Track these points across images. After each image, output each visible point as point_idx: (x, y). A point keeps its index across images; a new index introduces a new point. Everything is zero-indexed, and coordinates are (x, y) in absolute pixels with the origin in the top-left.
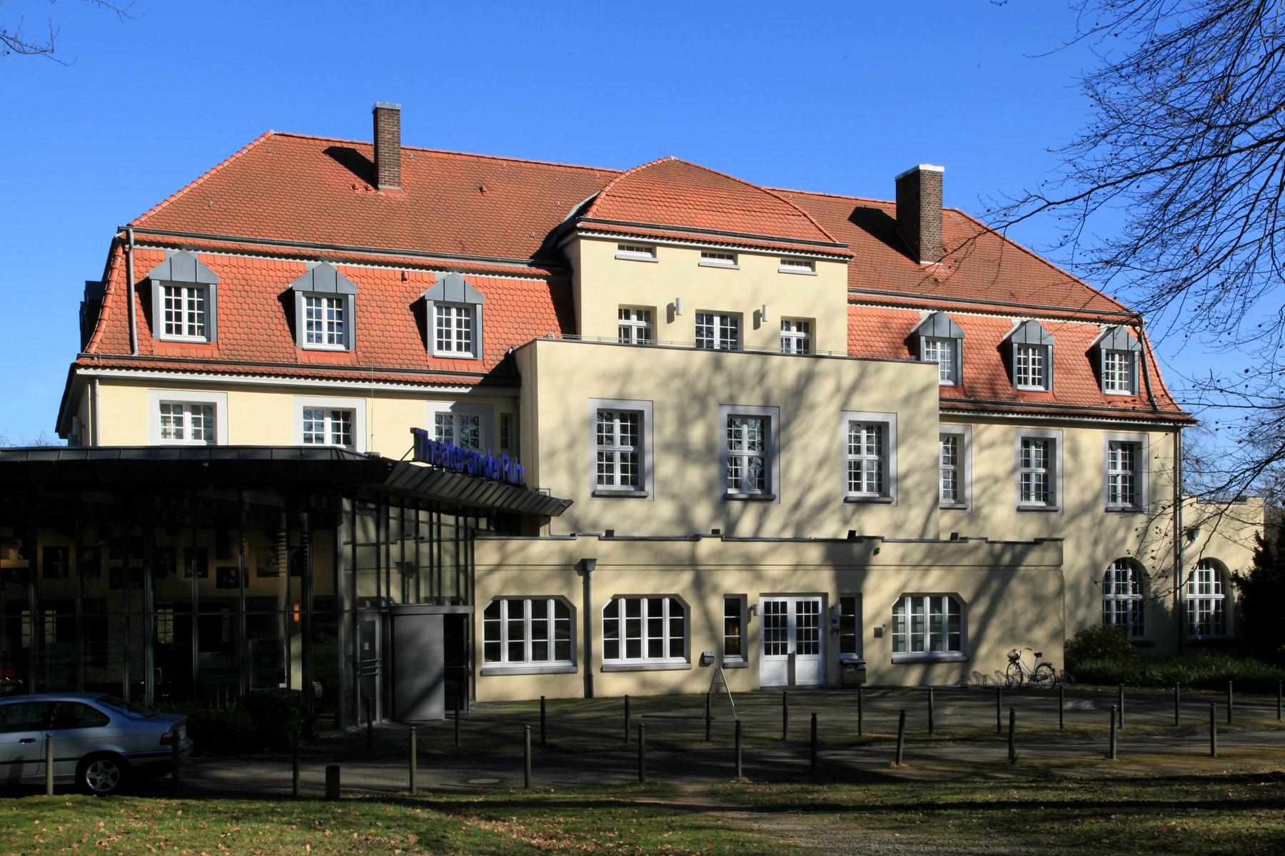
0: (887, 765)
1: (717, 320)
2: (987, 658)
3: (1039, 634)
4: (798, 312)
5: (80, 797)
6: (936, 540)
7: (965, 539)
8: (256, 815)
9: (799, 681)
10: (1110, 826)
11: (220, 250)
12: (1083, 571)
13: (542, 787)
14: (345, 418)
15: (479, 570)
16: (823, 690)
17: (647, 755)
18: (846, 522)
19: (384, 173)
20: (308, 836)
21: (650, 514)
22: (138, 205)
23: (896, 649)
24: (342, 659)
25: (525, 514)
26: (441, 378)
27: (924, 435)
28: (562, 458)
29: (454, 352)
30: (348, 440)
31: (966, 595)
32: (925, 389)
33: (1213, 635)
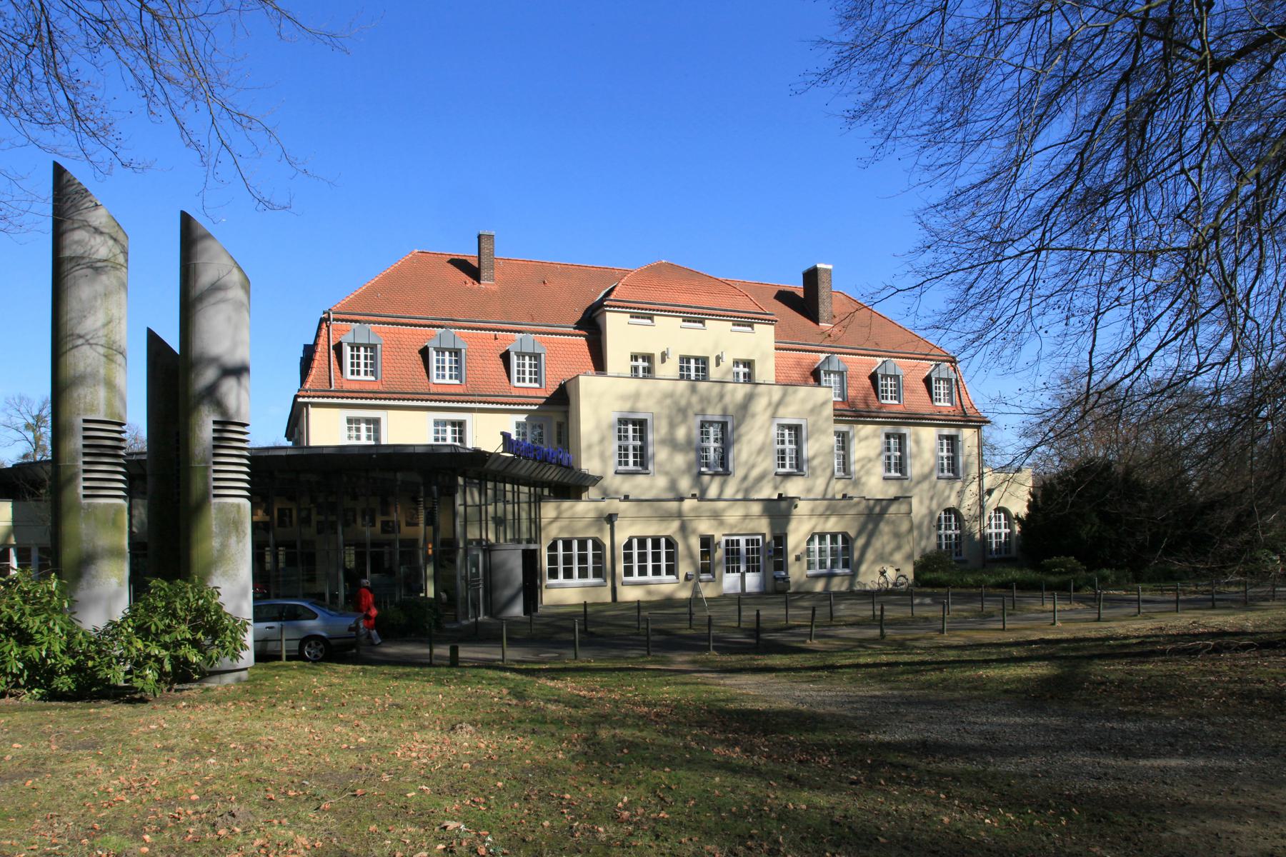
0: (804, 642)
1: (693, 361)
2: (865, 573)
3: (898, 557)
4: (744, 356)
5: (301, 663)
6: (833, 499)
7: (851, 498)
8: (408, 675)
9: (748, 590)
10: (942, 676)
11: (384, 323)
12: (925, 516)
13: (587, 658)
14: (460, 425)
15: (544, 521)
16: (764, 594)
17: (652, 638)
18: (776, 488)
19: (484, 274)
20: (440, 690)
21: (651, 484)
22: (337, 297)
23: (809, 568)
24: (459, 578)
25: (572, 486)
26: (519, 400)
27: (823, 432)
28: (596, 449)
29: (527, 384)
30: (461, 440)
31: (852, 533)
32: (825, 403)
33: (1003, 555)
